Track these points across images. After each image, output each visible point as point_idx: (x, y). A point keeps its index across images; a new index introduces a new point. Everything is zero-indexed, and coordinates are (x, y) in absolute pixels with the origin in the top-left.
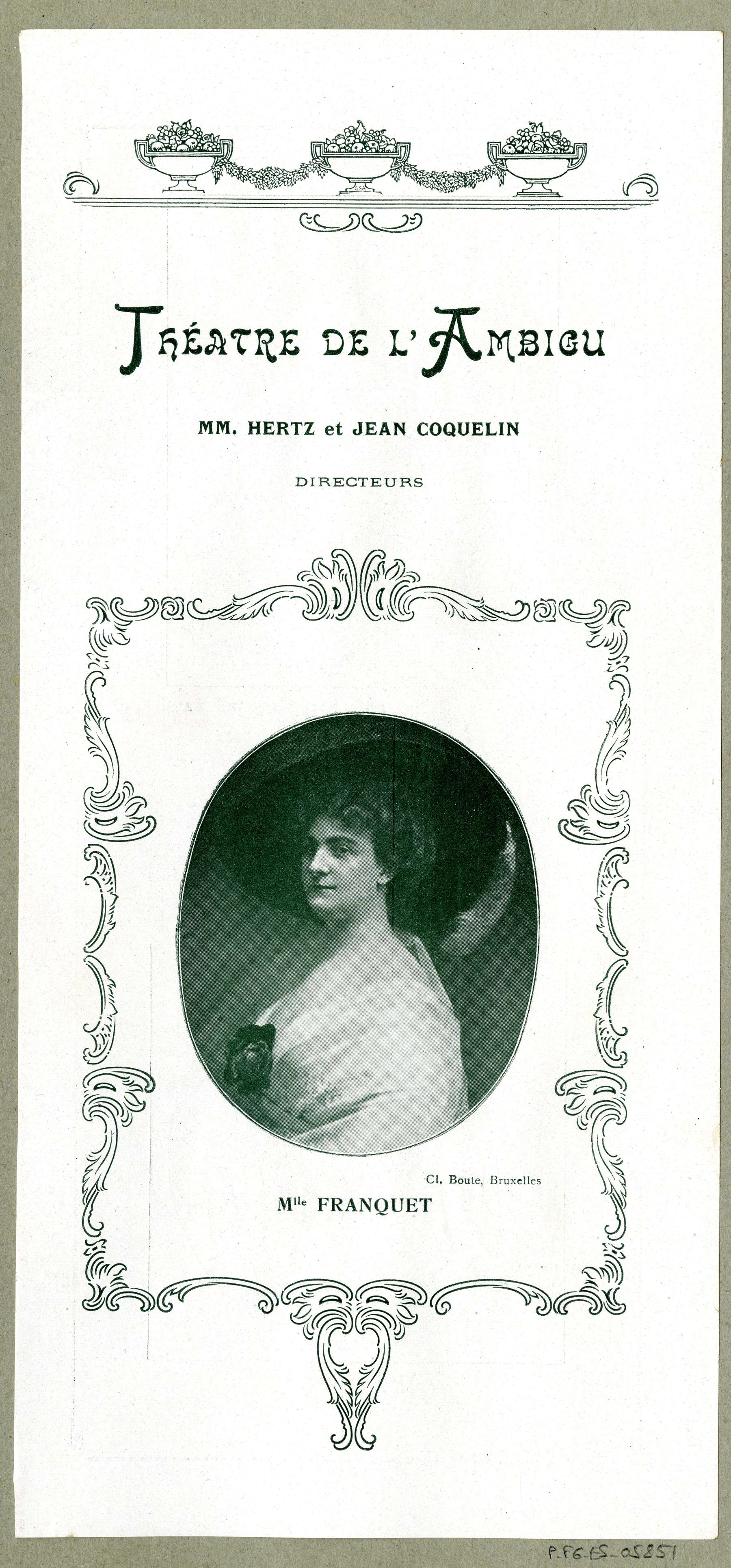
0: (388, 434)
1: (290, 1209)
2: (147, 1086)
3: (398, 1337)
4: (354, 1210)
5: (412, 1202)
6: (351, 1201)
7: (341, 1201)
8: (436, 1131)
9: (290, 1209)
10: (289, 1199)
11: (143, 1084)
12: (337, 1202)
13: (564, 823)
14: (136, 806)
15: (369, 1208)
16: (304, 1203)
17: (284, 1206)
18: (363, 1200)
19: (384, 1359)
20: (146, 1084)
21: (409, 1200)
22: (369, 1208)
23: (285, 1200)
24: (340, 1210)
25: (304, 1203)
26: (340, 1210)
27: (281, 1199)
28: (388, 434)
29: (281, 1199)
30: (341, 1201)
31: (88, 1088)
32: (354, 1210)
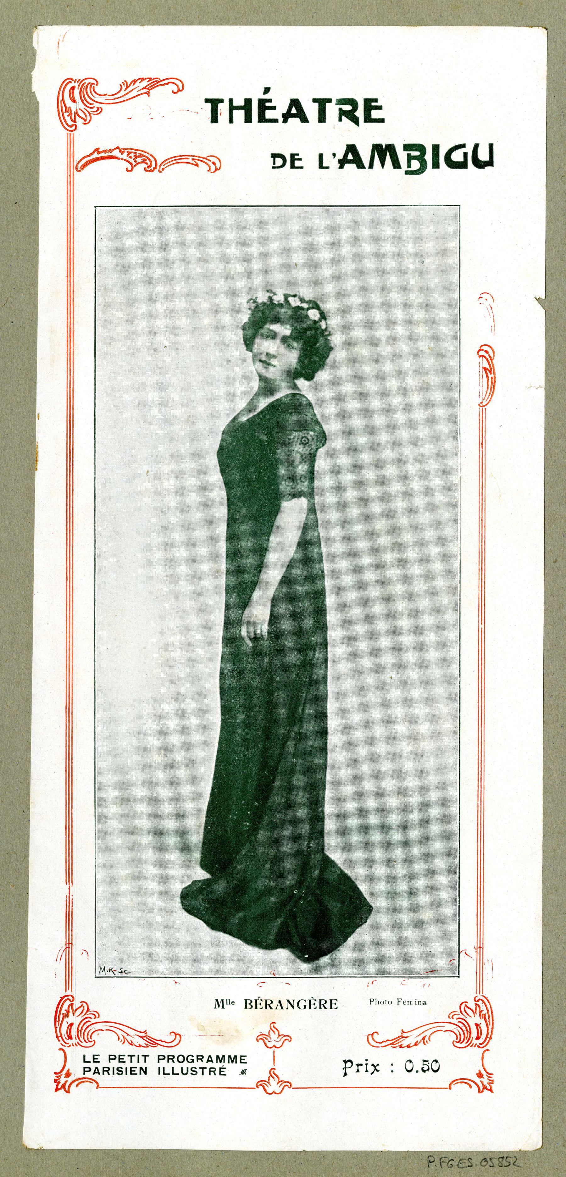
0: (304, 120)
1: (223, 1007)
2: (69, 999)
3: (97, 1016)
4: (282, 1008)
5: (334, 1002)
6: (280, 1002)
7: (251, 1002)
8: (455, 920)
9: (223, 1007)
10: (222, 1000)
11: (68, 1003)
12: (269, 1002)
13: (71, 999)
14: (84, 116)
15: (293, 1007)
16: (233, 1003)
17: (219, 1005)
18: (288, 1001)
19: (113, 1026)
20: (68, 1001)
21: (331, 1001)
22: (293, 1007)
23: (220, 1001)
24: (271, 1008)
25: (233, 1003)
26: (271, 1008)
27: (217, 1000)
28: (304, 120)
29: (217, 1000)
30: (272, 1002)
31: (70, 1044)
32: (282, 1008)
